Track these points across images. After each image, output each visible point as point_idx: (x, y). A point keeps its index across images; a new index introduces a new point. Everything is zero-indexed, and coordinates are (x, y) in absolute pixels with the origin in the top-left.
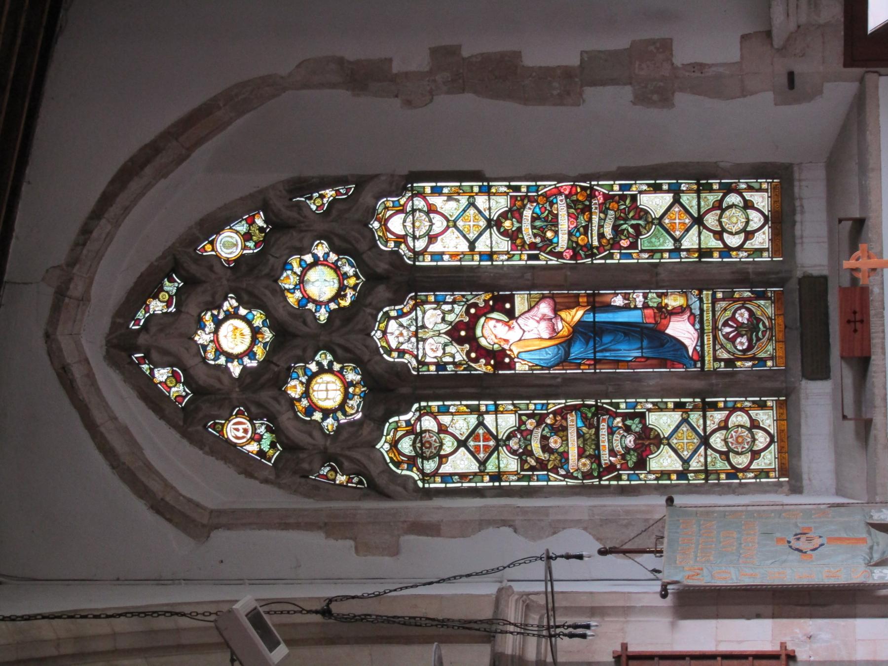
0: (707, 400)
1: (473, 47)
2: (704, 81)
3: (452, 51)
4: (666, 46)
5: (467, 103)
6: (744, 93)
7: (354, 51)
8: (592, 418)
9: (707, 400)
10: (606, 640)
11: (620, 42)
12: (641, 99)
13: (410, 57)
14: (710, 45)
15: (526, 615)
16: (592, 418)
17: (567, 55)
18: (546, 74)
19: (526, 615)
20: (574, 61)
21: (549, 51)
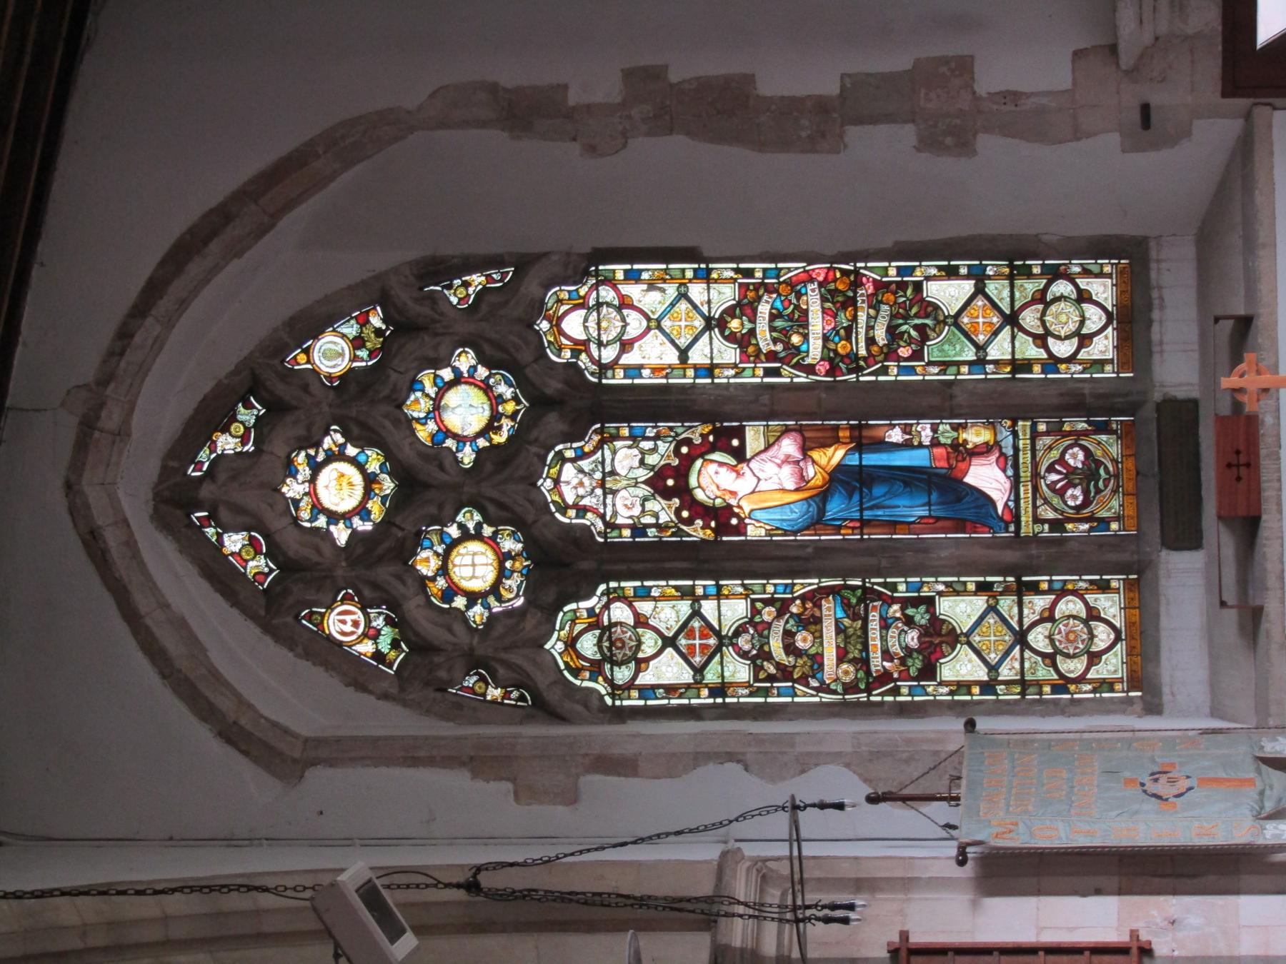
0: (1024, 579)
1: (686, 67)
2: (1020, 117)
3: (654, 74)
4: (964, 66)
5: (677, 149)
6: (1078, 134)
7: (513, 74)
8: (857, 605)
9: (1024, 579)
10: (877, 926)
11: (897, 61)
12: (928, 143)
13: (594, 82)
14: (1029, 65)
15: (762, 891)
16: (857, 605)
17: (821, 80)
18: (791, 106)
19: (762, 891)
20: (831, 88)
21: (796, 74)
